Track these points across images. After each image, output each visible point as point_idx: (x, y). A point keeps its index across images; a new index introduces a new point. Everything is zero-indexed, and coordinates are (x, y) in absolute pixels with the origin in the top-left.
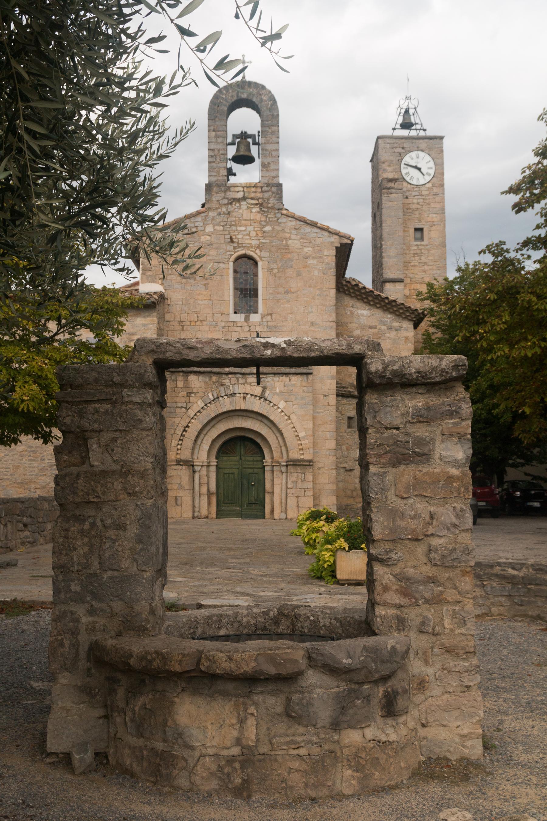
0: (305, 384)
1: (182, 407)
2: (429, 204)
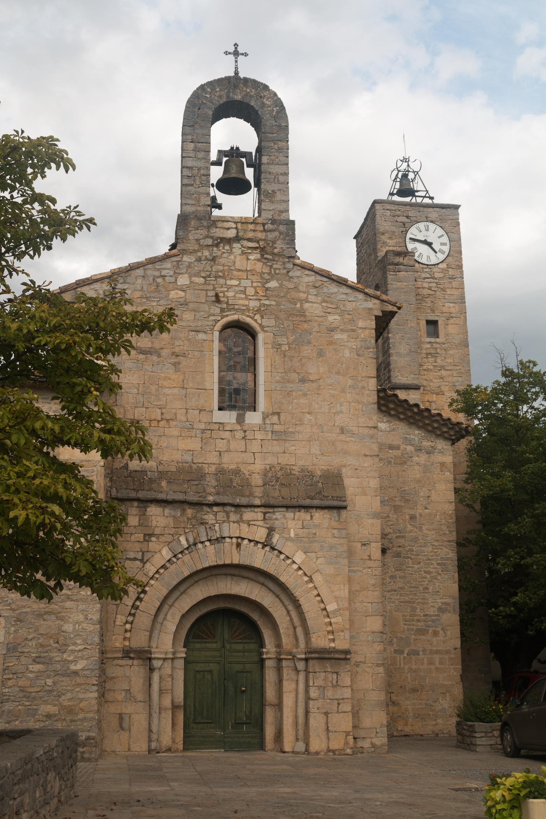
0: (334, 524)
1: (135, 559)
2: (443, 290)
